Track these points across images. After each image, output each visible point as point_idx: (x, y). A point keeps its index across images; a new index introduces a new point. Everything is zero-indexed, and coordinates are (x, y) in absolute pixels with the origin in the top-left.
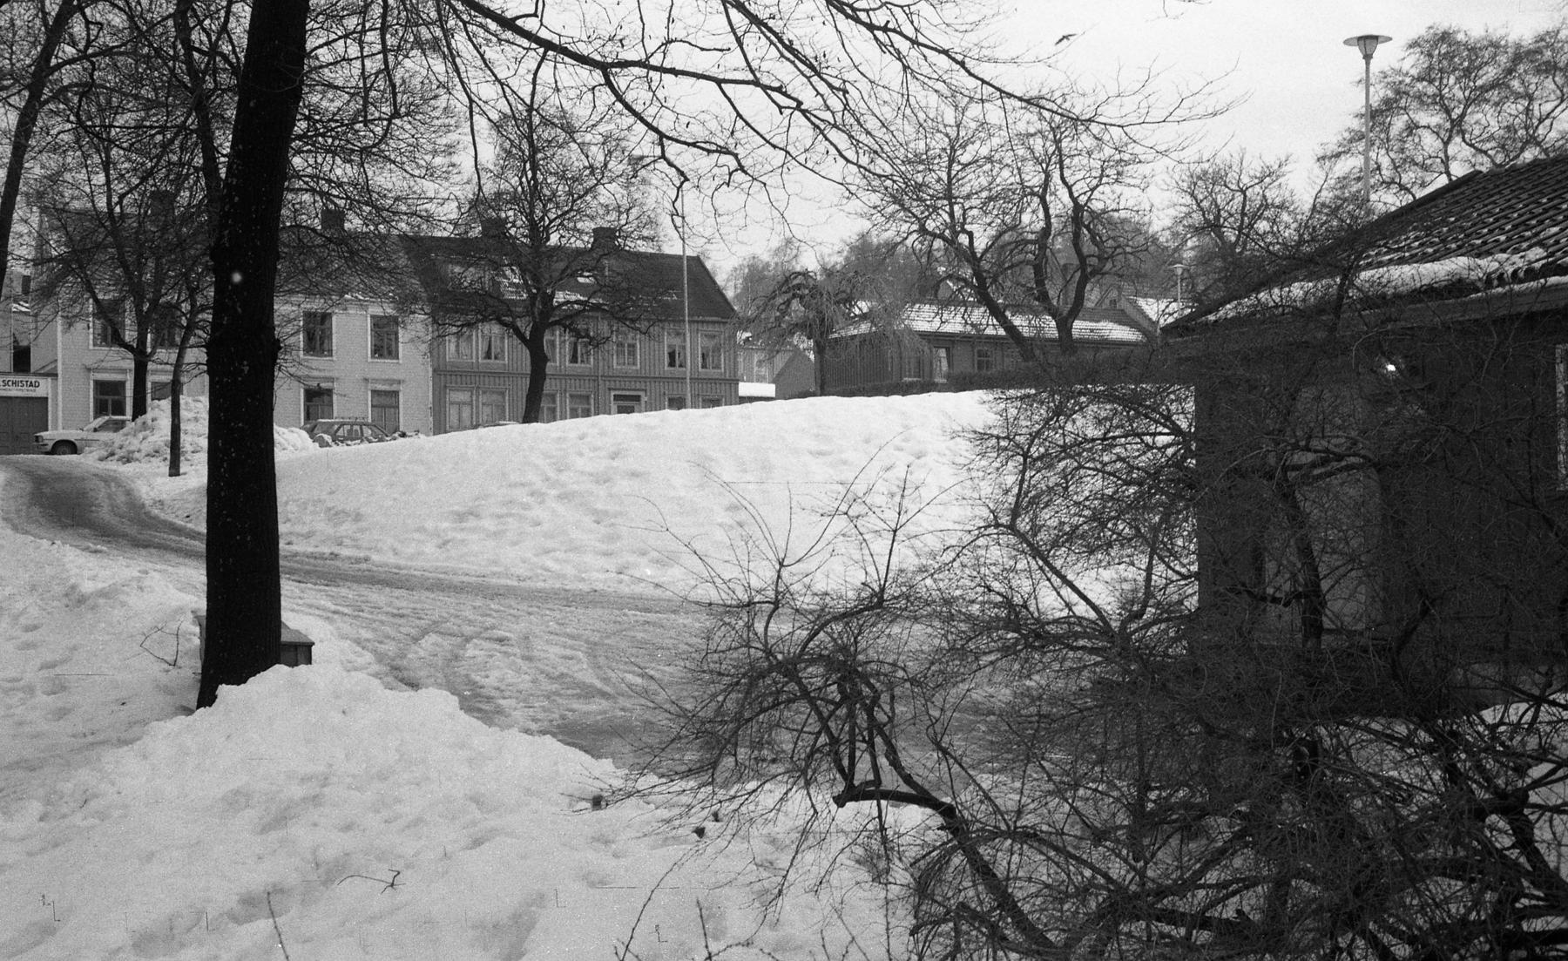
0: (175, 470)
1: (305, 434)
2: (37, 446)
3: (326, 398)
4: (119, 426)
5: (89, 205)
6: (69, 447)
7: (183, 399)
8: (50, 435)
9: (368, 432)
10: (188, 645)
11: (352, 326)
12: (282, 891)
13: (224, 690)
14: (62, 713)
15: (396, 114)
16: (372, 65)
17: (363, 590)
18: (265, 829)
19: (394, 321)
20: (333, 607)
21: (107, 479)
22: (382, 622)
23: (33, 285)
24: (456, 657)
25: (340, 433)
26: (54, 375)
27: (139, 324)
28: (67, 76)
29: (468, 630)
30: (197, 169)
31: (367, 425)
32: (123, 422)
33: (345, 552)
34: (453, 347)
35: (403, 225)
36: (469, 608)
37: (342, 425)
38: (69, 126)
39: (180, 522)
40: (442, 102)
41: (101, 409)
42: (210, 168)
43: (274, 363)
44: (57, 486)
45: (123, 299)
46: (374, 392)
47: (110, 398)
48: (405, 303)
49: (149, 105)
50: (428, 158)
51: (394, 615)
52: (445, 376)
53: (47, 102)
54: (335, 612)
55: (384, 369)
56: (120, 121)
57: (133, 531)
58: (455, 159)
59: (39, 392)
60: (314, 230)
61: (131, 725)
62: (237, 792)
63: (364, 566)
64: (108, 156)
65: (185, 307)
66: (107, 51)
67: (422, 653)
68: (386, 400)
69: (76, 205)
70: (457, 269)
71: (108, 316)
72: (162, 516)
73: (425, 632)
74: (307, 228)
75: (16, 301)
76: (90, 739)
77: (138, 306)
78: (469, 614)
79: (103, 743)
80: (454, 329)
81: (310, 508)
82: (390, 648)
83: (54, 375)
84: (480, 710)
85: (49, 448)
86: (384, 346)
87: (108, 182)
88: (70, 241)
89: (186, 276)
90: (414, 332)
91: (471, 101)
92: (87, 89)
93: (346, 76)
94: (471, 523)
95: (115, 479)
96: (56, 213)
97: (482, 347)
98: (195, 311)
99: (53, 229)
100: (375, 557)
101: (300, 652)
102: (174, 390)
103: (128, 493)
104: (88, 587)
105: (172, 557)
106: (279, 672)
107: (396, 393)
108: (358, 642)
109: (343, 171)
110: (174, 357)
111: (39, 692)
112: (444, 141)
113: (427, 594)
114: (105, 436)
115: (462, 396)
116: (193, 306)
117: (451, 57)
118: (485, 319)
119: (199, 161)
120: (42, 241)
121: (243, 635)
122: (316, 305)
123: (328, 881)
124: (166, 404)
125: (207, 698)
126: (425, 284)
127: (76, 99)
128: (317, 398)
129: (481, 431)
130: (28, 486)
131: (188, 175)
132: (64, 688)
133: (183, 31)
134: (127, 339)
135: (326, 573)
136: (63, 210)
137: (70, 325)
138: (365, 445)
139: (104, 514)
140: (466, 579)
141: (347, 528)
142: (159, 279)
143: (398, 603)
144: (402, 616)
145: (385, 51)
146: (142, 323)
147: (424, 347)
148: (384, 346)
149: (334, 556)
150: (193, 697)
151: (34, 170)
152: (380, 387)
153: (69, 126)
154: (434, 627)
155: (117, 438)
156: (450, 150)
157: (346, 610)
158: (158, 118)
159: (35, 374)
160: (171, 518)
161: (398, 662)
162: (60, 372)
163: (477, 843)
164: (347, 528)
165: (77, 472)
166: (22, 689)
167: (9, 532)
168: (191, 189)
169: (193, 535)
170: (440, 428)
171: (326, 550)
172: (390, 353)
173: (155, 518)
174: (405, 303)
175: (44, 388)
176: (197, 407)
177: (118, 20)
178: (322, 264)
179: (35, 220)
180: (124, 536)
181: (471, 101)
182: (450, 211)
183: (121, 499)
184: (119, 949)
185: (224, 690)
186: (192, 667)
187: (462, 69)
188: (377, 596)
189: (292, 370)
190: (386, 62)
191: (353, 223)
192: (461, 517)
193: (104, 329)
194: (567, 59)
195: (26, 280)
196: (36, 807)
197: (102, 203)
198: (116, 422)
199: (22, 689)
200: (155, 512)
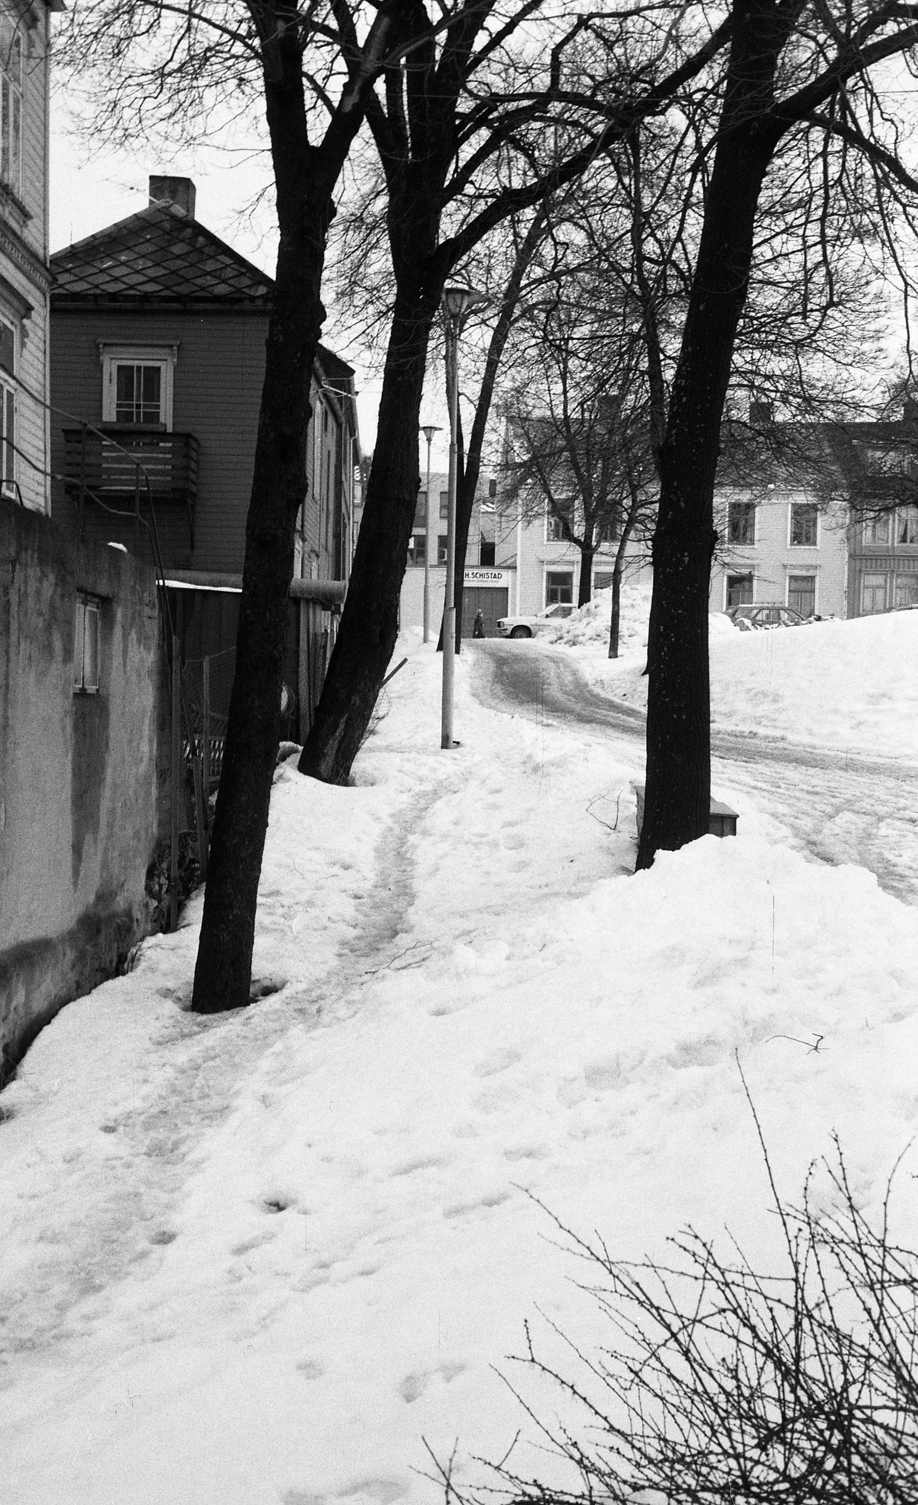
0: (613, 652)
1: (728, 619)
2: (499, 631)
3: (746, 584)
4: (567, 613)
5: (549, 413)
6: (524, 631)
7: (623, 588)
8: (510, 621)
9: (784, 616)
10: (627, 813)
11: (773, 518)
12: (714, 1043)
13: (661, 855)
14: (522, 866)
15: (831, 304)
16: (815, 255)
17: (780, 767)
18: (700, 984)
19: (814, 508)
20: (753, 783)
21: (555, 661)
22: (798, 799)
23: (499, 488)
24: (869, 836)
25: (759, 617)
26: (513, 568)
27: (587, 520)
28: (536, 296)
29: (882, 810)
30: (643, 373)
31: (785, 610)
32: (570, 609)
33: (761, 731)
34: (869, 532)
35: (828, 414)
36: (882, 787)
37: (761, 609)
38: (533, 341)
39: (617, 700)
40: (872, 289)
41: (552, 597)
42: (655, 372)
43: (711, 553)
44: (516, 667)
45: (574, 498)
46: (791, 577)
47: (559, 587)
48: (825, 492)
49: (602, 317)
50: (858, 344)
51: (808, 792)
52: (861, 561)
53: (516, 320)
54: (754, 788)
55: (803, 555)
56: (579, 332)
57: (578, 707)
58: (882, 344)
59: (501, 583)
60: (744, 424)
61: (579, 879)
62: (673, 949)
63: (781, 745)
64: (566, 367)
65: (627, 503)
66: (570, 272)
67: (837, 830)
68: (803, 585)
69: (537, 414)
70: (879, 454)
71: (560, 511)
72: (603, 694)
73: (838, 810)
74: (737, 422)
75: (484, 503)
76: (546, 890)
77: (586, 504)
78: (880, 793)
79: (557, 894)
80: (872, 514)
81: (732, 689)
82: (806, 824)
83: (513, 568)
84: (893, 887)
85: (509, 632)
86: (803, 533)
87: (565, 392)
88: (531, 448)
89: (629, 474)
90: (832, 521)
91: (907, 284)
92: (552, 306)
93: (791, 269)
94: (885, 705)
95: (562, 660)
96: (519, 421)
97: (898, 530)
98: (636, 506)
99: (517, 436)
100: (791, 737)
101: (726, 824)
102: (615, 579)
103: (574, 673)
104: (540, 757)
105: (610, 731)
106: (709, 839)
107: (812, 578)
108: (774, 815)
109: (778, 365)
110: (616, 550)
111: (502, 848)
112: (873, 326)
113: (839, 772)
114: (556, 621)
115: (878, 580)
116: (634, 501)
117: (889, 243)
118: (903, 503)
119: (644, 365)
120: (508, 449)
121: (676, 808)
122: (745, 497)
123: (755, 1038)
124: (608, 592)
125: (645, 861)
126: (847, 471)
127: (543, 316)
128: (740, 584)
129: (894, 614)
130: (492, 666)
131: (634, 380)
132: (522, 845)
133: (638, 243)
134: (576, 535)
135: (747, 751)
136: (526, 419)
137: (529, 522)
138: (783, 628)
139: (554, 692)
140: (881, 761)
141: (765, 708)
142: (607, 476)
143: (815, 782)
144: (817, 793)
145: (823, 242)
146: (589, 519)
147: (841, 533)
148: (803, 533)
149: (754, 735)
150: (631, 860)
151: (505, 382)
152: (797, 572)
153: (533, 341)
154: (849, 805)
155: (565, 623)
156: (877, 335)
157: (764, 786)
158: (613, 326)
159: (499, 567)
160: (611, 697)
161: (814, 837)
162: (518, 565)
163: (898, 1017)
164: (765, 708)
165: (532, 655)
166: (489, 844)
167: (477, 706)
168: (636, 393)
169: (631, 713)
170: (854, 612)
171: (746, 728)
172: (808, 539)
173: (596, 696)
174: (825, 492)
175: (505, 580)
176: (639, 595)
177: (580, 238)
178: (751, 456)
179: (502, 428)
180: (571, 712)
181: (907, 284)
182: (879, 397)
183: (568, 678)
184: (574, 1079)
185: (661, 855)
186: (630, 831)
187: (899, 253)
188: (792, 773)
189: (727, 560)
190: (825, 254)
191: (782, 415)
192: (875, 699)
193: (557, 525)
194: (654, 256)
195: (493, 483)
196: (503, 948)
197: (559, 411)
198: (564, 609)
199: (489, 844)
200: (597, 690)
